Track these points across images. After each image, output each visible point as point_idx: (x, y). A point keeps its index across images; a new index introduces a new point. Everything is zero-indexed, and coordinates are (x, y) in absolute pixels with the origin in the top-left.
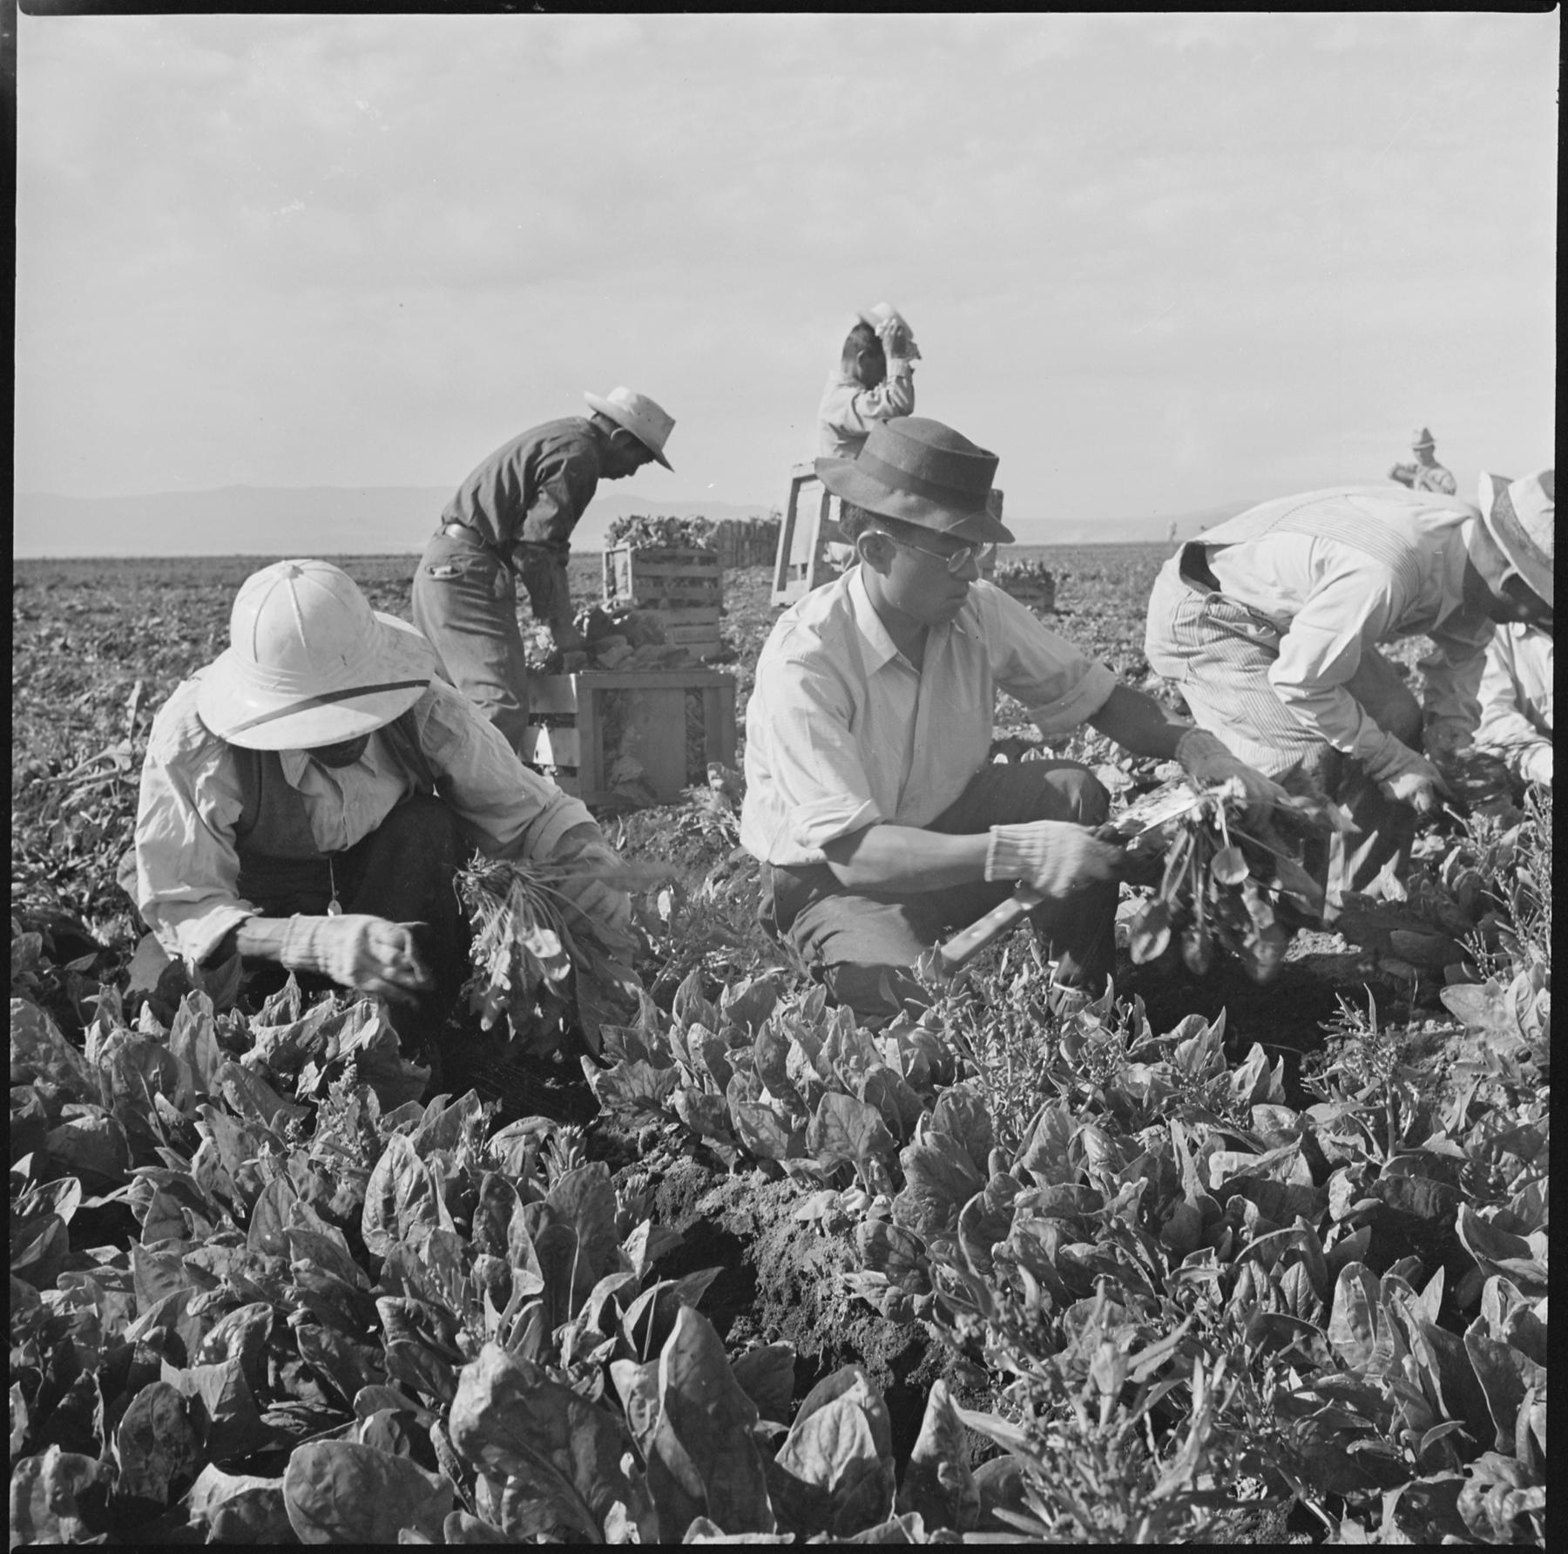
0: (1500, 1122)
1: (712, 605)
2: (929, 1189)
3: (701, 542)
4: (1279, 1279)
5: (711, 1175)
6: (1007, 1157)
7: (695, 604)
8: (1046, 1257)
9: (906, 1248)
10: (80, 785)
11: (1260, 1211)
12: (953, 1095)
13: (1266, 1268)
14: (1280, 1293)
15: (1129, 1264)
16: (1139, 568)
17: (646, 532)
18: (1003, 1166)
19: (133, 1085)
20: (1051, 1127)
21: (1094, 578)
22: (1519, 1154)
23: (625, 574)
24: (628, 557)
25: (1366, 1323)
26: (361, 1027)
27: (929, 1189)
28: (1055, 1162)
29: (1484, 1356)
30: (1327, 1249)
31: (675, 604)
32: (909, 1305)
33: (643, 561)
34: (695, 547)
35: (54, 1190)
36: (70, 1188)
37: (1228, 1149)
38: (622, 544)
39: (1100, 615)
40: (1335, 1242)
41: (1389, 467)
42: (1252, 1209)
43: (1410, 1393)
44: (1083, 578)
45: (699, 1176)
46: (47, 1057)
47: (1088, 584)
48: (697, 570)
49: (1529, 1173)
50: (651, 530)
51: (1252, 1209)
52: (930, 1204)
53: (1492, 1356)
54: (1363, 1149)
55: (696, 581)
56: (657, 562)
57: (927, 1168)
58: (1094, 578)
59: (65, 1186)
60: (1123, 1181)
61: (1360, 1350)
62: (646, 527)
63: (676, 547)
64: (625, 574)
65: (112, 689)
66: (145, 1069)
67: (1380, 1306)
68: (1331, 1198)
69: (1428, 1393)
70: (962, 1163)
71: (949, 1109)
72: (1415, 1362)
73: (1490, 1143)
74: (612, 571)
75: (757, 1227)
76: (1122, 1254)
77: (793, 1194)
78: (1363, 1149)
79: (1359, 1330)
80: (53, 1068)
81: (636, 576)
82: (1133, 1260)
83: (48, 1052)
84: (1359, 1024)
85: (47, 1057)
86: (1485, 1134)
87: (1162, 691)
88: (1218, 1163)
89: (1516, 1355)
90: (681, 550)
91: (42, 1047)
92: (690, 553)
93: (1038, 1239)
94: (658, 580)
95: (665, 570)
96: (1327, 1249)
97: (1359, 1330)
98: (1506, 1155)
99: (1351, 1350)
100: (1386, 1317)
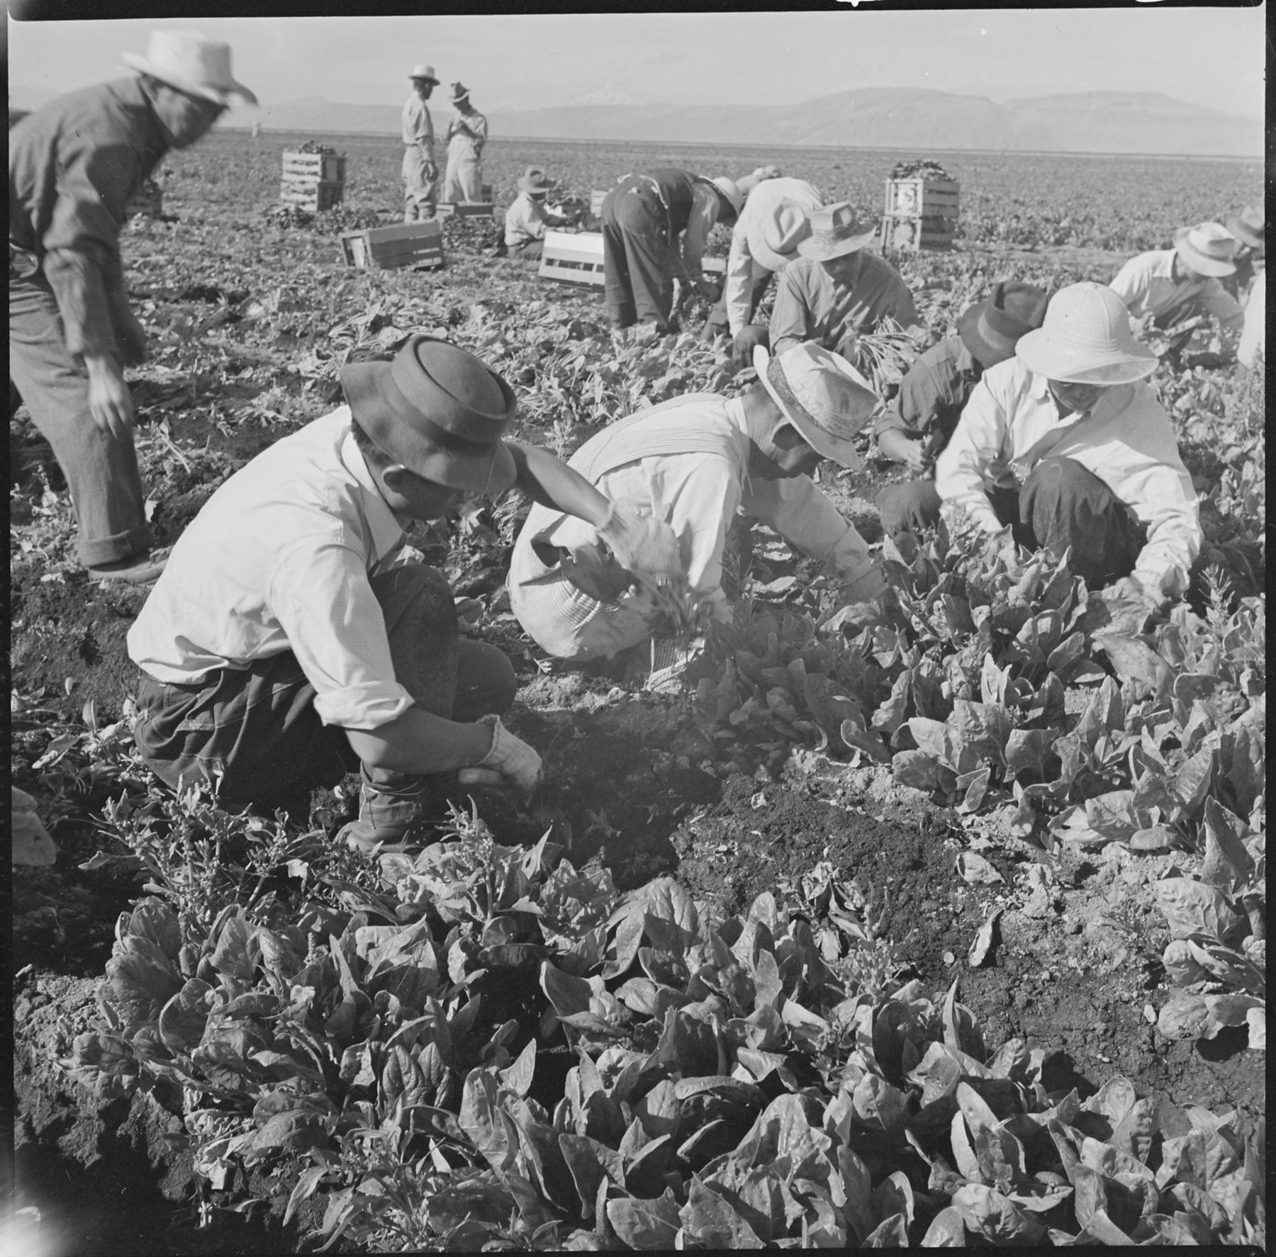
0: (566, 876)
2: (133, 992)
4: (417, 1055)
6: (195, 952)
8: (236, 1054)
9: (116, 1049)
11: (401, 1003)
12: (146, 907)
13: (407, 1049)
14: (418, 1067)
15: (301, 1047)
16: (231, 167)
18: (193, 962)
20: (232, 934)
22: (580, 898)
25: (486, 1112)
27: (133, 992)
28: (236, 958)
29: (572, 1146)
30: (449, 1017)
32: (119, 1084)
37: (370, 924)
39: (202, 222)
40: (456, 1012)
41: (434, 66)
42: (394, 1001)
43: (521, 1186)
44: (184, 175)
47: (189, 181)
49: (586, 912)
51: (394, 1001)
52: (134, 1004)
53: (578, 1146)
54: (469, 911)
57: (128, 973)
58: (193, 176)
60: (294, 984)
61: (483, 1132)
67: (496, 1108)
68: (450, 963)
69: (534, 1180)
70: (158, 959)
71: (143, 917)
72: (524, 1158)
73: (559, 891)
76: (296, 1042)
78: (469, 911)
79: (482, 1119)
82: (304, 1045)
84: (465, 823)
86: (556, 886)
87: (263, 321)
88: (362, 937)
89: (594, 1143)
93: (229, 1045)
96: (449, 1017)
97: (482, 1119)
98: (569, 900)
99: (476, 1133)
100: (500, 1115)
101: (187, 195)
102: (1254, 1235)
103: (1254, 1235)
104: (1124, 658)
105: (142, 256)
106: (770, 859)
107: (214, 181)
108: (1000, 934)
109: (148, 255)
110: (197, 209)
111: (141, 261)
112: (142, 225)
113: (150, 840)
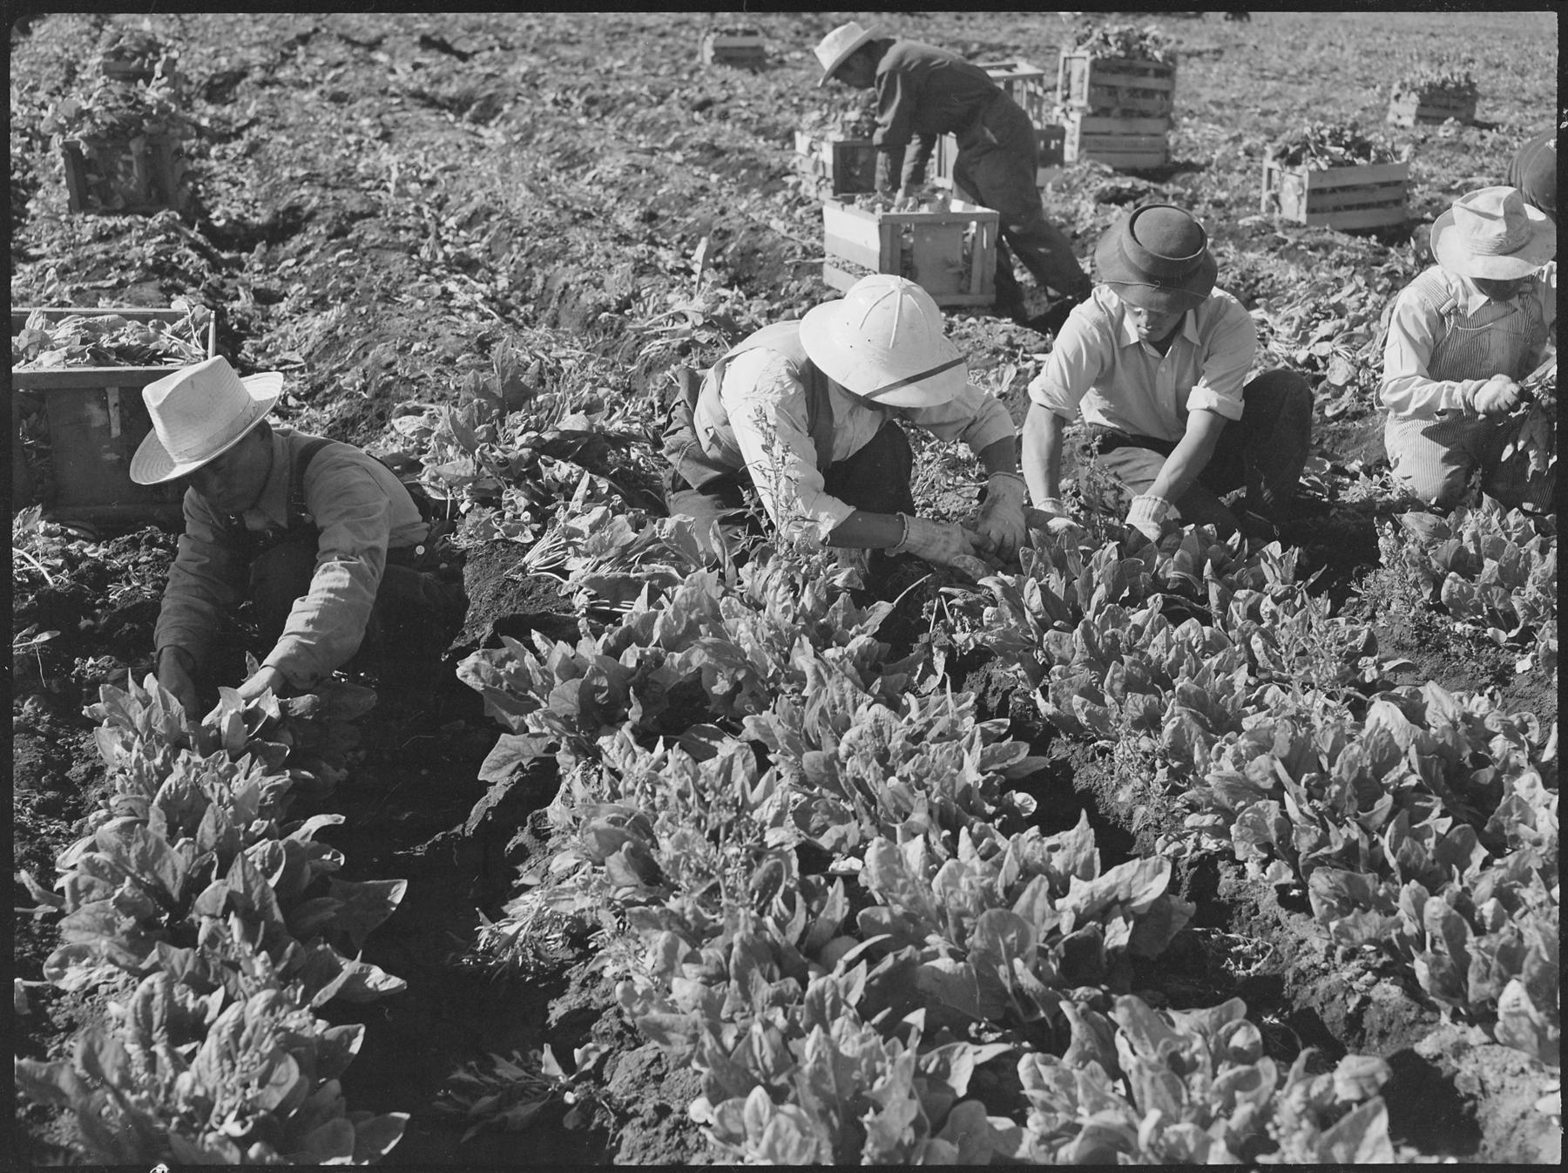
1: (1162, 116)
3: (1158, 55)
5: (1421, 1012)
7: (1145, 115)
10: (657, 336)
17: (1106, 42)
19: (993, 944)
21: (1498, 66)
23: (1082, 81)
24: (1087, 65)
26: (1152, 879)
31: (1127, 114)
33: (1100, 70)
34: (1152, 60)
35: (950, 1051)
36: (963, 1052)
38: (1082, 51)
45: (1409, 1010)
46: (903, 890)
47: (1492, 72)
48: (1151, 82)
50: (1111, 40)
55: (1148, 93)
56: (1114, 72)
58: (1498, 66)
59: (959, 1050)
62: (1106, 36)
63: (1134, 58)
64: (1082, 81)
65: (618, 172)
66: (1004, 933)
74: (1068, 76)
75: (1483, 1091)
77: (1523, 1071)
80: (905, 898)
81: (1092, 84)
83: (904, 886)
85: (903, 890)
90: (1139, 63)
91: (900, 882)
92: (1145, 64)
94: (1113, 90)
95: (1121, 81)
101: (1493, 91)
102: (1551, 1154)
103: (1551, 1154)
104: (1541, 49)
105: (1463, 176)
106: (1263, 351)
107: (1522, 73)
108: (1146, 170)
109: (1470, 176)
110: (1512, 113)
111: (1461, 182)
112: (1452, 131)
113: (1198, 531)
